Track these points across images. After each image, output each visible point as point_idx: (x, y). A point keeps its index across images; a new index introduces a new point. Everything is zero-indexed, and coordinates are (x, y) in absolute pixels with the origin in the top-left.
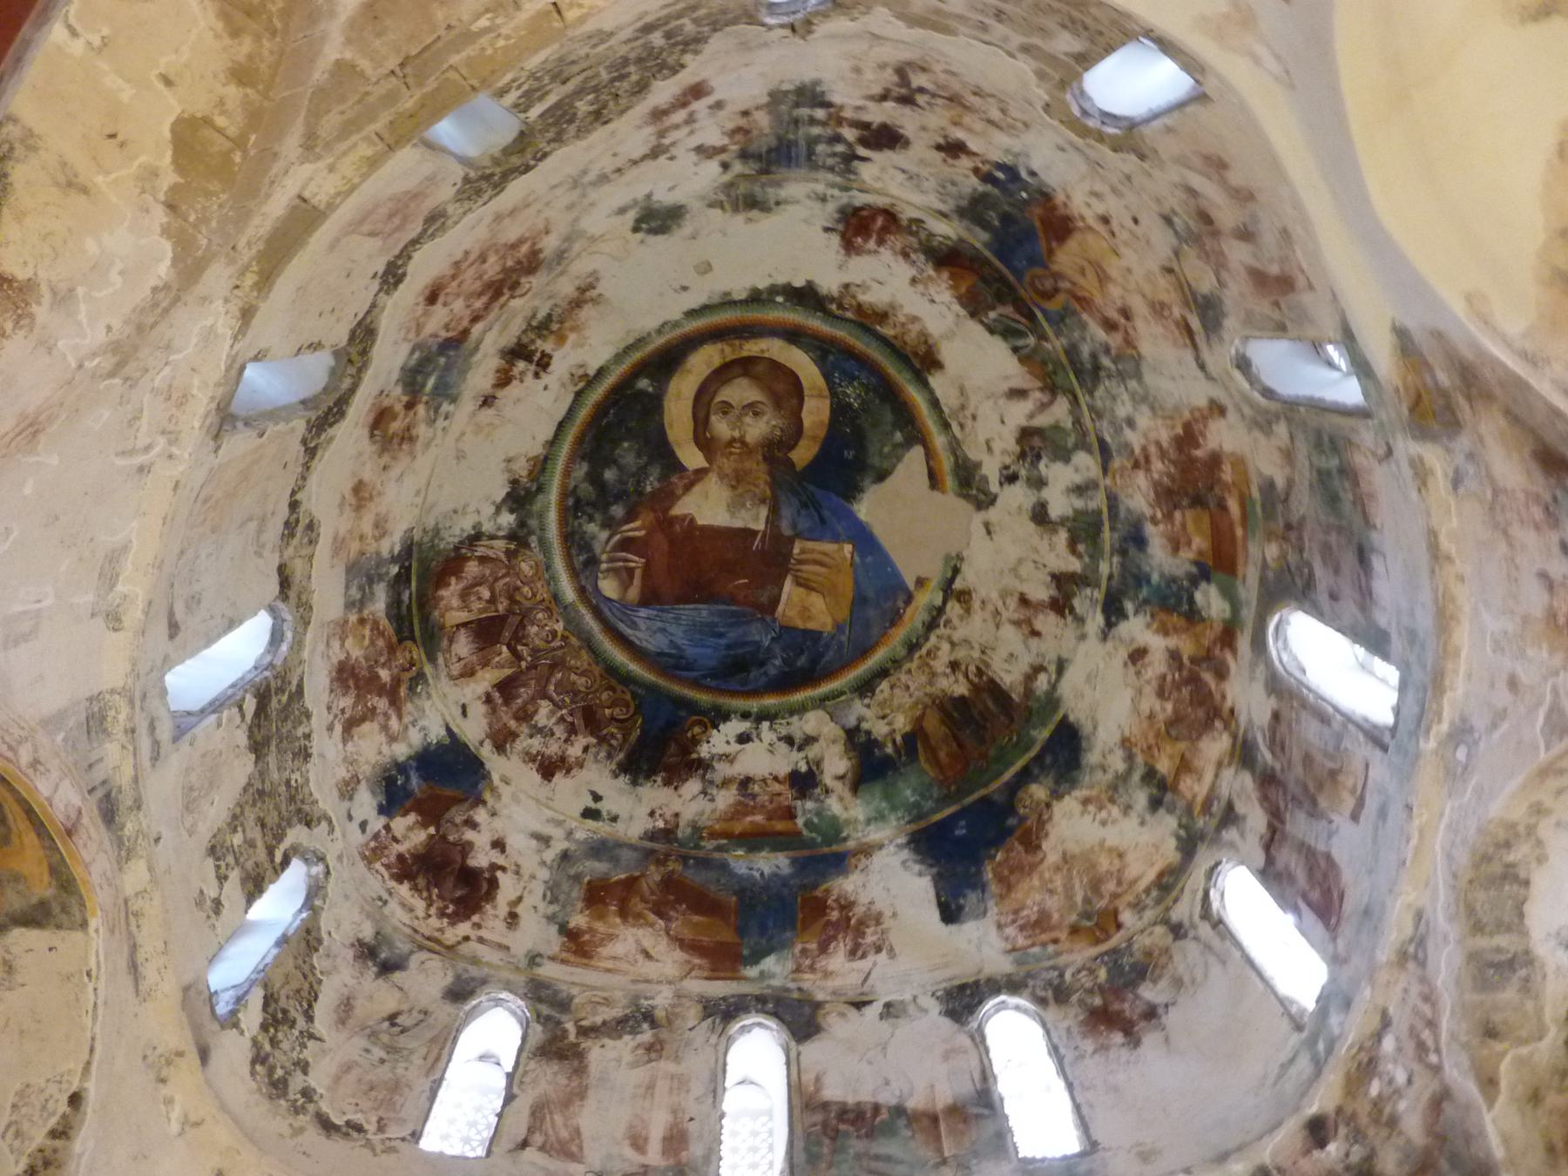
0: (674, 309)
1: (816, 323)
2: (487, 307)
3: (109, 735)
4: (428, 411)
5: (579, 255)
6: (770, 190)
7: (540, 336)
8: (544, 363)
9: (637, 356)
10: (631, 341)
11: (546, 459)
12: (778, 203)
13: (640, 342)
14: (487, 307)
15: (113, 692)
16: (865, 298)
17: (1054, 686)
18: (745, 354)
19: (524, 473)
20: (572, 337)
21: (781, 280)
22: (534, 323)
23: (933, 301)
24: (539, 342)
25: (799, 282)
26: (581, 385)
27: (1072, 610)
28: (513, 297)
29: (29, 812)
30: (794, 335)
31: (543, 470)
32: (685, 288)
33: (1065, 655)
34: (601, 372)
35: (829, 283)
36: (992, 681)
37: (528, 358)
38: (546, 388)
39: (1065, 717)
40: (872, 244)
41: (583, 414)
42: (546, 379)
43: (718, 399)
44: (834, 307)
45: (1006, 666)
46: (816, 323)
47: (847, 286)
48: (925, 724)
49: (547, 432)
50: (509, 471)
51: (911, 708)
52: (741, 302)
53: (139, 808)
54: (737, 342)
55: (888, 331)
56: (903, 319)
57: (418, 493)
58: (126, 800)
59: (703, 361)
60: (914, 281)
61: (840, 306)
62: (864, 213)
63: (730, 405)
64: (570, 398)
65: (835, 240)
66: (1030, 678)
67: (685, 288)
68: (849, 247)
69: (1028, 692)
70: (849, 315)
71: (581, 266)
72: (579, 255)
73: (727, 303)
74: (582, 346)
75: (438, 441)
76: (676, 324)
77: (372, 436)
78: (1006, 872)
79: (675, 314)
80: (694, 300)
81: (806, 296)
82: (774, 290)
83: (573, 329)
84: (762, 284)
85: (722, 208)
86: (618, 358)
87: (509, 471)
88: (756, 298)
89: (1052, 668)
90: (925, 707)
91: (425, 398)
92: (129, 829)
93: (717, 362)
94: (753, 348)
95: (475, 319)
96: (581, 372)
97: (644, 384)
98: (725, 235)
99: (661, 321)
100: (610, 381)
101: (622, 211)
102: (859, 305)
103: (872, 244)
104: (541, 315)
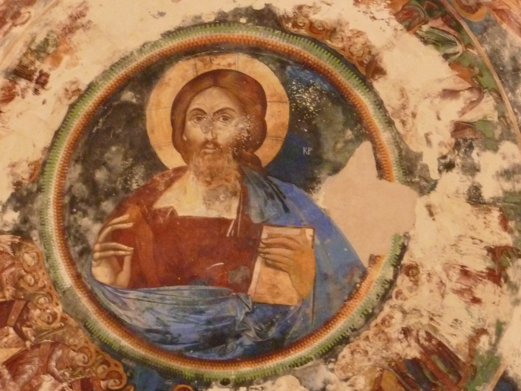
0: (153, 32)
1: (274, 39)
8: (42, 81)
9: (121, 72)
11: (45, 163)
13: (124, 60)
17: (494, 346)
18: (214, 68)
20: (66, 58)
22: (33, 47)
23: (374, 18)
24: (38, 63)
26: (74, 98)
27: (507, 279)
28: (14, 25)
30: (256, 50)
31: (42, 173)
32: (162, 14)
33: (503, 319)
34: (91, 87)
36: (440, 344)
38: (44, 102)
39: (505, 373)
41: (76, 123)
44: (290, 25)
45: (452, 330)
46: (274, 39)
48: (383, 385)
49: (46, 140)
51: (370, 371)
52: (210, 24)
54: (208, 58)
56: (349, 34)
66: (473, 340)
67: (162, 14)
69: (472, 353)
70: (303, 32)
76: (155, 44)
79: (154, 35)
82: (237, 13)
86: (105, 75)
88: (222, 20)
89: (492, 330)
90: (382, 370)
93: (191, 75)
94: (221, 62)
96: (74, 87)
97: (128, 96)
99: (141, 43)
102: (311, 24)
104: (40, 39)
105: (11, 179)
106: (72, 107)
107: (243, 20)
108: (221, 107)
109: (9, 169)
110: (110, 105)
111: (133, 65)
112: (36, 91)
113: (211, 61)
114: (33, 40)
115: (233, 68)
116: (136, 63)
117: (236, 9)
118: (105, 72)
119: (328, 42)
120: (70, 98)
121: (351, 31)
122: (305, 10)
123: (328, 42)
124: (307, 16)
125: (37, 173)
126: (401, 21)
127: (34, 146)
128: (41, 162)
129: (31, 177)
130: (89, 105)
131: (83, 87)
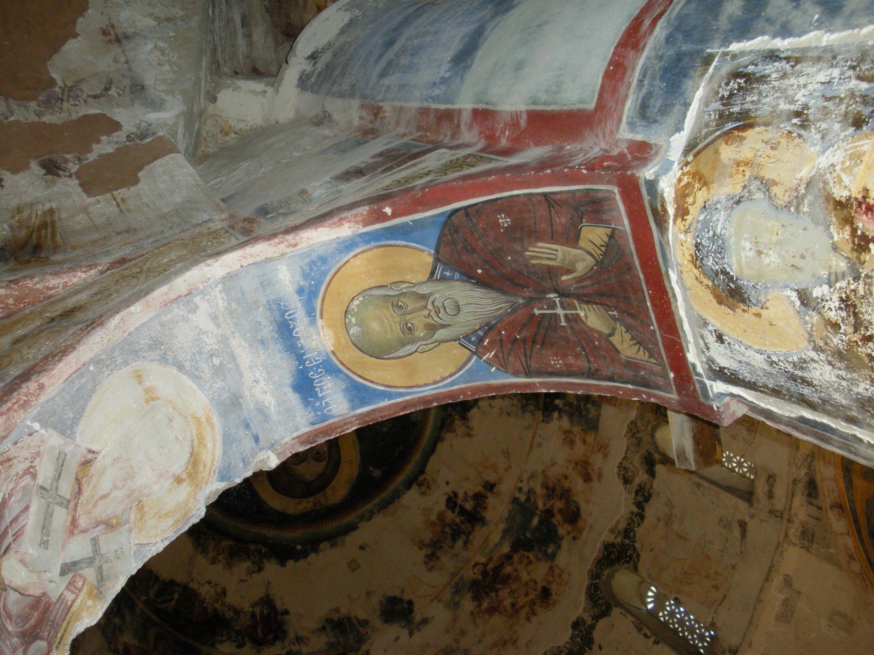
0: (365, 532)
1: (271, 533)
2: (501, 566)
3: (801, 524)
4: (535, 503)
5: (445, 588)
6: (333, 640)
7: (457, 525)
8: (452, 501)
9: (385, 495)
10: (391, 507)
11: (442, 428)
12: (324, 628)
13: (384, 505)
14: (501, 566)
15: (795, 544)
16: (247, 564)
18: (311, 499)
19: (457, 422)
20: (433, 517)
21: (302, 563)
22: (464, 537)
23: (209, 582)
24: (458, 520)
25: (290, 563)
26: (421, 478)
28: (485, 565)
29: (859, 532)
30: (283, 520)
31: (443, 420)
32: (362, 548)
34: (408, 485)
35: (271, 567)
37: (463, 511)
38: (447, 483)
40: (257, 610)
41: (417, 457)
42: (449, 489)
43: (324, 463)
44: (263, 550)
46: (271, 533)
47: (260, 570)
49: (443, 448)
50: (468, 427)
52: (323, 541)
53: (795, 480)
54: (318, 508)
55: (225, 543)
56: (220, 557)
57: (540, 445)
58: (800, 488)
59: (338, 490)
60: (224, 593)
61: (259, 551)
62: (271, 636)
63: (314, 459)
64: (429, 468)
65: (279, 606)
67: (362, 548)
68: (267, 601)
70: (253, 547)
71: (438, 578)
72: (445, 588)
73: (333, 538)
74: (425, 509)
75: (525, 477)
76: (362, 518)
77: (578, 508)
78: (216, 361)
79: (364, 526)
80: (353, 539)
81: (284, 554)
82: (304, 554)
83: (433, 524)
84: (312, 556)
85: (358, 620)
86: (396, 496)
87: (468, 427)
88: (312, 545)
91: (538, 512)
92: (803, 471)
93: (329, 491)
94: (306, 505)
95: (509, 557)
96: (423, 489)
97: (377, 473)
98: (349, 596)
99: (372, 521)
100: (401, 478)
101: (425, 621)
102: (248, 557)
103: (257, 610)
104: (460, 543)
105: (470, 424)
106: (422, 471)
107: (299, 547)
108: (303, 465)
109: (473, 433)
110: (392, 469)
111: (377, 501)
112: (455, 495)
113: (315, 505)
114: (465, 543)
115: (297, 500)
116: (244, 355)
117: (306, 557)
118: (399, 497)
119: (232, 543)
120: (425, 479)
121: (220, 562)
122: (256, 569)
123: (232, 543)
124: (254, 563)
125: (448, 422)
126: (193, 590)
127: (452, 446)
128: (445, 430)
129: (453, 420)
130: (409, 469)
131: (415, 486)
